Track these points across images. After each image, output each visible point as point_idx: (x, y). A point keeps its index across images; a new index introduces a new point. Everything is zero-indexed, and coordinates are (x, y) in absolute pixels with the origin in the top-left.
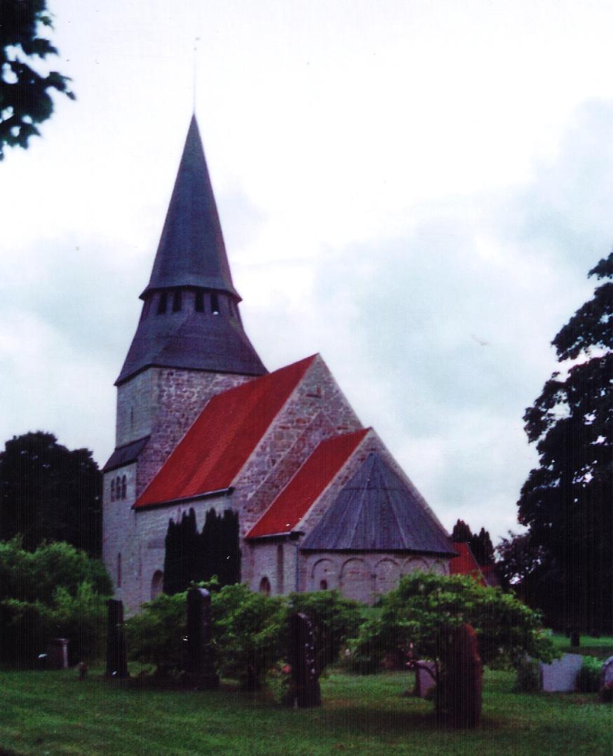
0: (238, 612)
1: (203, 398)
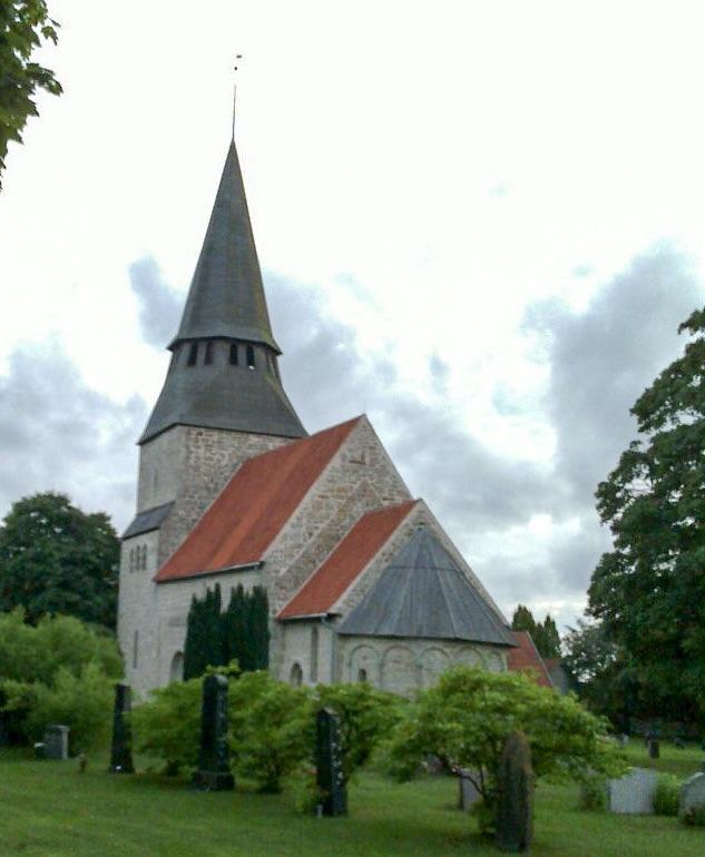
0: (258, 703)
1: (235, 461)
